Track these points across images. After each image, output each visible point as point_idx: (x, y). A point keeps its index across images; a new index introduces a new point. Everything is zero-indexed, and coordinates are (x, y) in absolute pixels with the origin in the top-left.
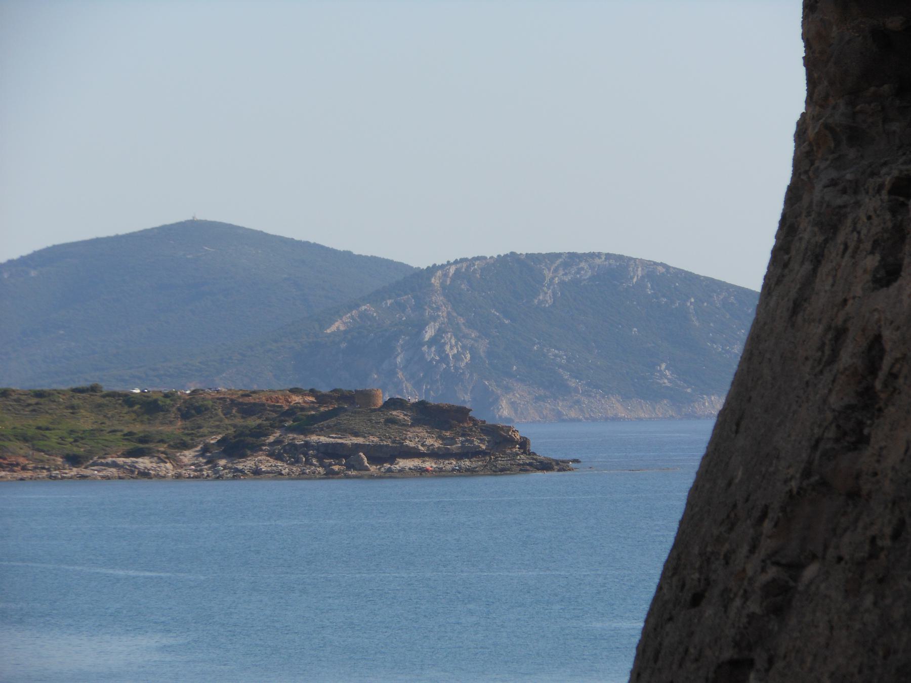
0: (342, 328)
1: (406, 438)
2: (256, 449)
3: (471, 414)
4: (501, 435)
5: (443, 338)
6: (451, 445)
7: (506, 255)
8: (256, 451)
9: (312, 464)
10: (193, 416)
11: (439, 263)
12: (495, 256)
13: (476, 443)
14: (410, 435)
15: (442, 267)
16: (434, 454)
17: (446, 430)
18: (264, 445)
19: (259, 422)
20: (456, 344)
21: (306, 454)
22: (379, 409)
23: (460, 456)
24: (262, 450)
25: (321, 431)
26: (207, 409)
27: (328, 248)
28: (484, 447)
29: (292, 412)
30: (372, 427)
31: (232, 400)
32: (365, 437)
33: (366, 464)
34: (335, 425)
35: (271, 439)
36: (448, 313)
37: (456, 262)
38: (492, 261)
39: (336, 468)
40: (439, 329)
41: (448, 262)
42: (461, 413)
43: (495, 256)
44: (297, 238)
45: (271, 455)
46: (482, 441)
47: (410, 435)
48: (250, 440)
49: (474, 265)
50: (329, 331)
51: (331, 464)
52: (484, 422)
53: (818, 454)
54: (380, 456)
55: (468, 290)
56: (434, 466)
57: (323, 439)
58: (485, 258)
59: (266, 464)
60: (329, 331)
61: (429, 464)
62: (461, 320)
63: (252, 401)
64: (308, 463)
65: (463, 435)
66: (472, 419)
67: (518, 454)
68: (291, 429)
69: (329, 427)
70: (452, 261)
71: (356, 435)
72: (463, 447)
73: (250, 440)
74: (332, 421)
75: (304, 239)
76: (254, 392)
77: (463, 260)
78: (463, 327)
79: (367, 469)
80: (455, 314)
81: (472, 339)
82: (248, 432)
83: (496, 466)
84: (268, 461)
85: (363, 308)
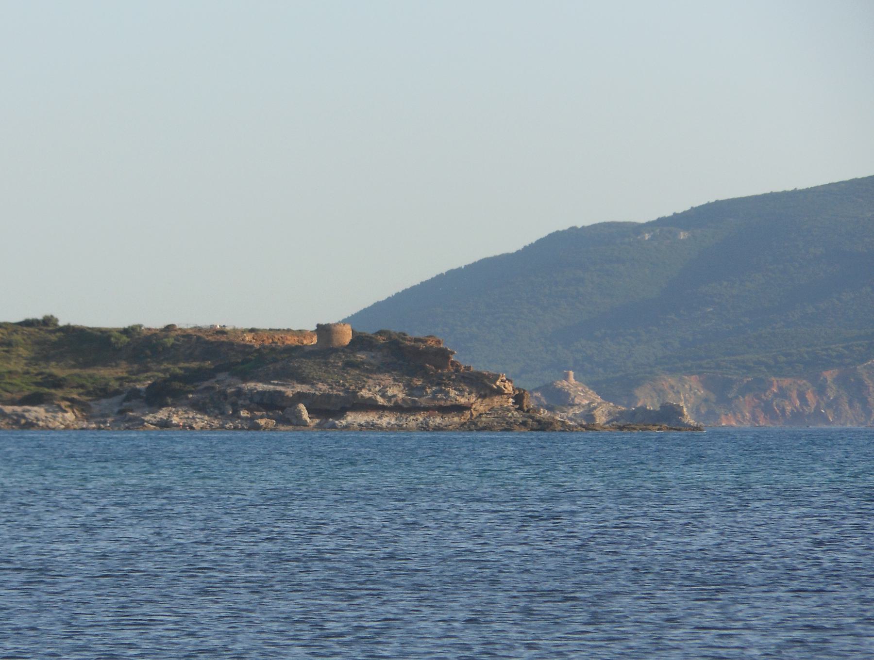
1: (364, 387)
6: (419, 397)
16: (398, 408)
31: (199, 338)
32: (313, 384)
39: (262, 422)
46: (461, 392)
57: (261, 387)
65: (438, 384)
67: (509, 410)
71: (303, 381)
72: (434, 398)
79: (305, 424)
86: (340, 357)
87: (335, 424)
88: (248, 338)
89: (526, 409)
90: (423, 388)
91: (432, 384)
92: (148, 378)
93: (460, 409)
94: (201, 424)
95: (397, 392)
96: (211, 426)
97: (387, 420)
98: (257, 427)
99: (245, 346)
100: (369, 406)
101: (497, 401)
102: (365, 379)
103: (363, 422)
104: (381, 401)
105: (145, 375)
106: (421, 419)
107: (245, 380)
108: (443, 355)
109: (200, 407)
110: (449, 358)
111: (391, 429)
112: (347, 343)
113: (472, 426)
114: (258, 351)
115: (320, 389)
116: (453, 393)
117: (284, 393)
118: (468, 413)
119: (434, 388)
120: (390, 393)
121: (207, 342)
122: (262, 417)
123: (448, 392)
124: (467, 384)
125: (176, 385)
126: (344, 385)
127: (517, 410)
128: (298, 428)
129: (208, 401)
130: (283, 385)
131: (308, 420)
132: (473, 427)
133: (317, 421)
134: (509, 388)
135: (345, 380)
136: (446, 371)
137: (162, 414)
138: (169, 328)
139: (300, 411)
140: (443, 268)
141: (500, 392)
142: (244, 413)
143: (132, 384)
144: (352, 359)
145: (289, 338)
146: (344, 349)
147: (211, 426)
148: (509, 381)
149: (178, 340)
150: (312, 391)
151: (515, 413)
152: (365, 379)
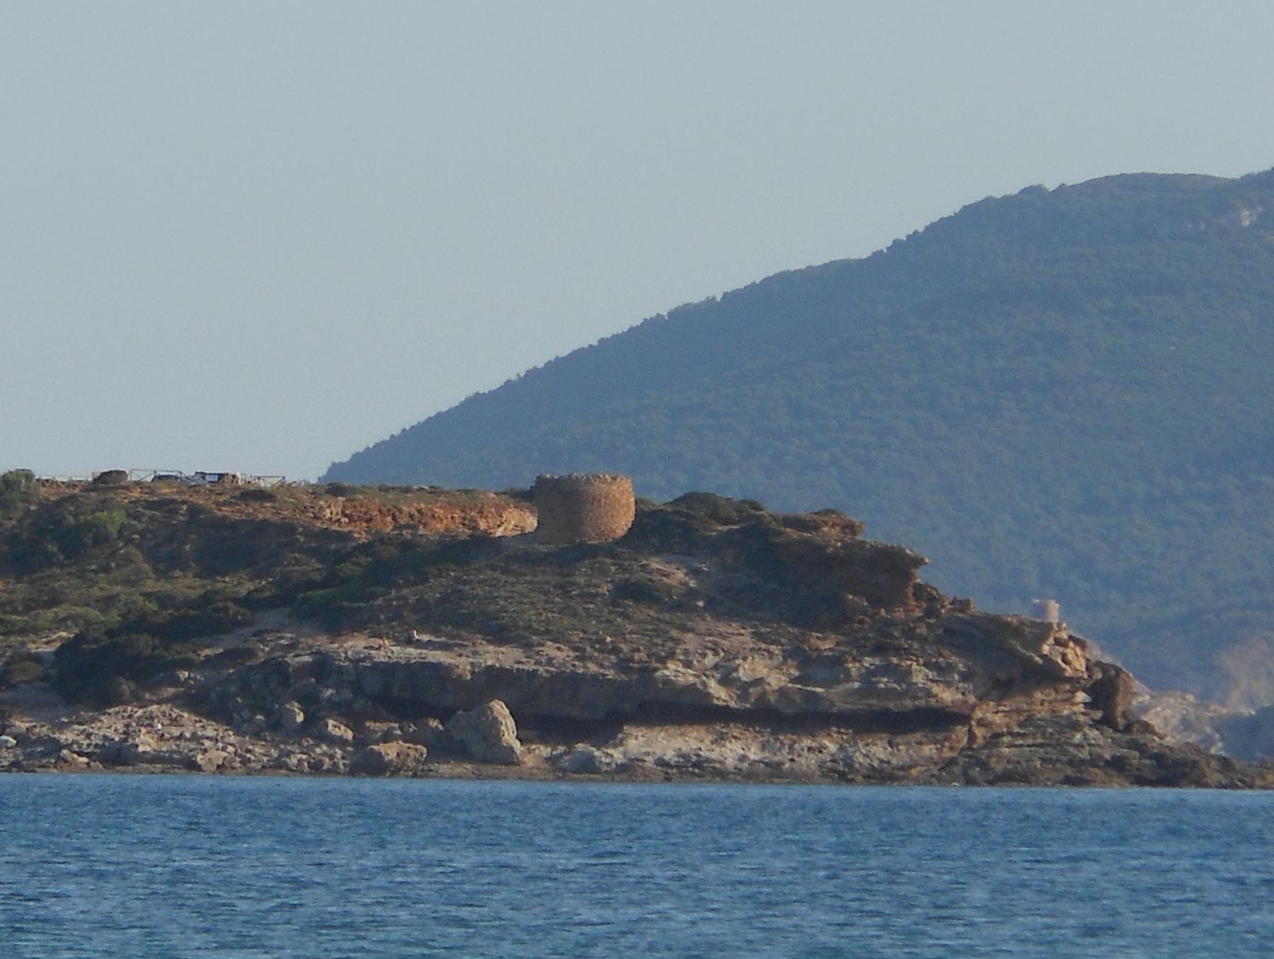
1: (671, 655)
3: (920, 576)
4: (1012, 654)
6: (827, 684)
10: (49, 560)
16: (764, 716)
18: (187, 665)
21: (309, 701)
25: (395, 624)
26: (101, 539)
30: (566, 611)
31: (194, 510)
32: (527, 646)
39: (390, 751)
46: (943, 671)
52: (963, 605)
53: (42, 837)
54: (571, 716)
57: (389, 651)
65: (878, 650)
66: (921, 592)
67: (1076, 726)
71: (499, 636)
72: (869, 689)
79: (508, 758)
84: (175, 722)
86: (604, 572)
87: (591, 758)
88: (332, 510)
89: (1121, 722)
90: (837, 662)
91: (863, 650)
92: (60, 623)
93: (938, 720)
94: (218, 756)
95: (767, 671)
96: (245, 761)
97: (738, 749)
98: (376, 767)
99: (325, 533)
100: (689, 709)
101: (1041, 701)
102: (674, 633)
103: (670, 755)
104: (720, 694)
105: (50, 614)
106: (832, 748)
107: (335, 629)
108: (892, 568)
109: (202, 703)
110: (908, 576)
111: (748, 775)
112: (620, 532)
113: (974, 768)
114: (364, 549)
115: (550, 661)
116: (920, 676)
117: (449, 669)
118: (961, 731)
119: (868, 661)
120: (745, 672)
121: (221, 524)
122: (387, 738)
123: (909, 672)
124: (960, 650)
125: (144, 642)
126: (616, 650)
127: (1096, 724)
128: (489, 769)
129: (233, 689)
130: (445, 647)
131: (517, 745)
132: (976, 772)
133: (544, 751)
134: (1076, 662)
135: (619, 634)
136: (899, 614)
137: (109, 726)
138: (108, 481)
139: (495, 723)
140: (661, 300)
141: (1050, 675)
142: (335, 727)
143: (14, 640)
144: (639, 576)
145: (439, 512)
146: (613, 549)
147: (245, 761)
148: (1078, 642)
149: (136, 516)
150: (530, 667)
151: (1093, 734)
152: (674, 633)
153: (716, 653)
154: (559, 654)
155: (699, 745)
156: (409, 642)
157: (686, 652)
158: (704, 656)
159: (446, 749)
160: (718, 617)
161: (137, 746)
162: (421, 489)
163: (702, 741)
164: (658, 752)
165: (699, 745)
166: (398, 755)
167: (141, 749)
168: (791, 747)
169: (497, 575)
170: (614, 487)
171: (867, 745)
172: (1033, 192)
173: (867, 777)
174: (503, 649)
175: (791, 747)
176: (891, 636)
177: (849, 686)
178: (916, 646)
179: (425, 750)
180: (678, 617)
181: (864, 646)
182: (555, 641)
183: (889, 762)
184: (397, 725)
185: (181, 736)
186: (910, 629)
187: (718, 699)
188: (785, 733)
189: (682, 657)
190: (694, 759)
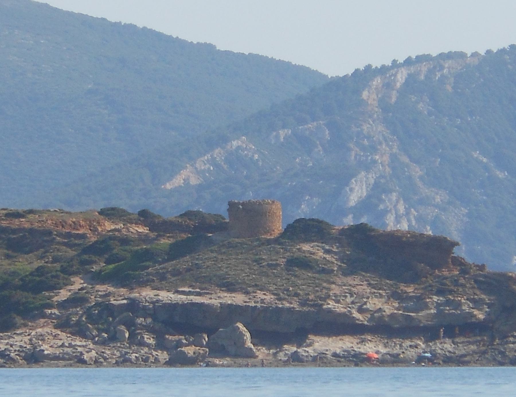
0: (194, 181)
1: (328, 297)
2: (32, 313)
3: (457, 252)
5: (381, 201)
6: (416, 311)
7: (502, 51)
8: (34, 318)
9: (142, 344)
11: (376, 64)
12: (482, 52)
13: (465, 308)
14: (335, 290)
15: (383, 70)
16: (382, 328)
17: (408, 282)
18: (51, 306)
19: (37, 264)
20: (408, 213)
21: (130, 325)
22: (276, 241)
23: (430, 333)
24: (44, 316)
25: (161, 281)
27: (169, 38)
28: (481, 316)
29: (102, 247)
32: (247, 293)
33: (249, 344)
34: (189, 270)
35: (64, 295)
36: (394, 158)
37: (408, 62)
38: (476, 61)
39: (190, 351)
40: (376, 185)
41: (394, 61)
42: (438, 249)
43: (482, 52)
44: (112, 18)
45: (63, 325)
46: (477, 303)
47: (335, 290)
48: (21, 296)
49: (442, 68)
50: (169, 186)
51: (179, 344)
52: (482, 267)
55: (430, 114)
56: (383, 350)
57: (166, 296)
58: (461, 55)
59: (51, 338)
60: (169, 186)
61: (372, 347)
62: (417, 171)
63: (27, 226)
64: (135, 341)
65: (440, 292)
66: (458, 262)
68: (99, 278)
69: (176, 273)
70: (401, 60)
71: (230, 287)
72: (440, 313)
73: (21, 296)
74: (183, 263)
75: (125, 20)
76: (31, 212)
77: (420, 59)
78: (420, 184)
80: (405, 159)
81: (436, 206)
82: (17, 281)
83: (503, 353)
85: (235, 143)
117: (208, 306)
126: (297, 295)
128: (240, 361)
130: (199, 294)
144: (297, 254)
150: (252, 304)
153: (352, 296)
154: (265, 297)
155: (351, 345)
156: (177, 292)
157: (336, 295)
158: (346, 296)
159: (219, 350)
160: (345, 274)
161: (43, 351)
162: (55, 211)
163: (353, 343)
164: (333, 350)
165: (351, 345)
166: (194, 353)
167: (46, 352)
168: (401, 346)
169: (214, 255)
170: (274, 207)
171: (441, 343)
172: (104, 19)
173: (444, 362)
174: (233, 295)
175: (401, 346)
176: (445, 285)
177: (428, 312)
178: (461, 289)
179: (207, 350)
180: (323, 276)
181: (432, 290)
182: (261, 290)
183: (454, 353)
184: (183, 337)
185: (63, 345)
186: (455, 280)
187: (358, 320)
188: (396, 338)
189: (334, 298)
190: (353, 353)
